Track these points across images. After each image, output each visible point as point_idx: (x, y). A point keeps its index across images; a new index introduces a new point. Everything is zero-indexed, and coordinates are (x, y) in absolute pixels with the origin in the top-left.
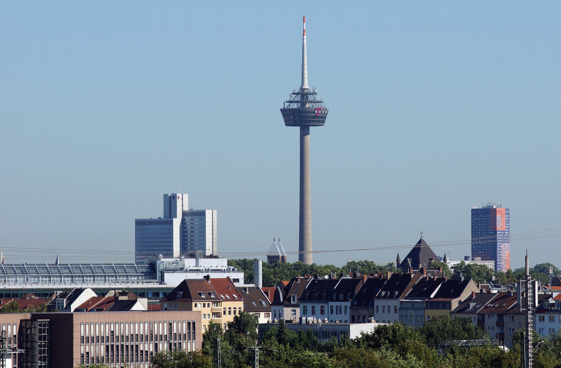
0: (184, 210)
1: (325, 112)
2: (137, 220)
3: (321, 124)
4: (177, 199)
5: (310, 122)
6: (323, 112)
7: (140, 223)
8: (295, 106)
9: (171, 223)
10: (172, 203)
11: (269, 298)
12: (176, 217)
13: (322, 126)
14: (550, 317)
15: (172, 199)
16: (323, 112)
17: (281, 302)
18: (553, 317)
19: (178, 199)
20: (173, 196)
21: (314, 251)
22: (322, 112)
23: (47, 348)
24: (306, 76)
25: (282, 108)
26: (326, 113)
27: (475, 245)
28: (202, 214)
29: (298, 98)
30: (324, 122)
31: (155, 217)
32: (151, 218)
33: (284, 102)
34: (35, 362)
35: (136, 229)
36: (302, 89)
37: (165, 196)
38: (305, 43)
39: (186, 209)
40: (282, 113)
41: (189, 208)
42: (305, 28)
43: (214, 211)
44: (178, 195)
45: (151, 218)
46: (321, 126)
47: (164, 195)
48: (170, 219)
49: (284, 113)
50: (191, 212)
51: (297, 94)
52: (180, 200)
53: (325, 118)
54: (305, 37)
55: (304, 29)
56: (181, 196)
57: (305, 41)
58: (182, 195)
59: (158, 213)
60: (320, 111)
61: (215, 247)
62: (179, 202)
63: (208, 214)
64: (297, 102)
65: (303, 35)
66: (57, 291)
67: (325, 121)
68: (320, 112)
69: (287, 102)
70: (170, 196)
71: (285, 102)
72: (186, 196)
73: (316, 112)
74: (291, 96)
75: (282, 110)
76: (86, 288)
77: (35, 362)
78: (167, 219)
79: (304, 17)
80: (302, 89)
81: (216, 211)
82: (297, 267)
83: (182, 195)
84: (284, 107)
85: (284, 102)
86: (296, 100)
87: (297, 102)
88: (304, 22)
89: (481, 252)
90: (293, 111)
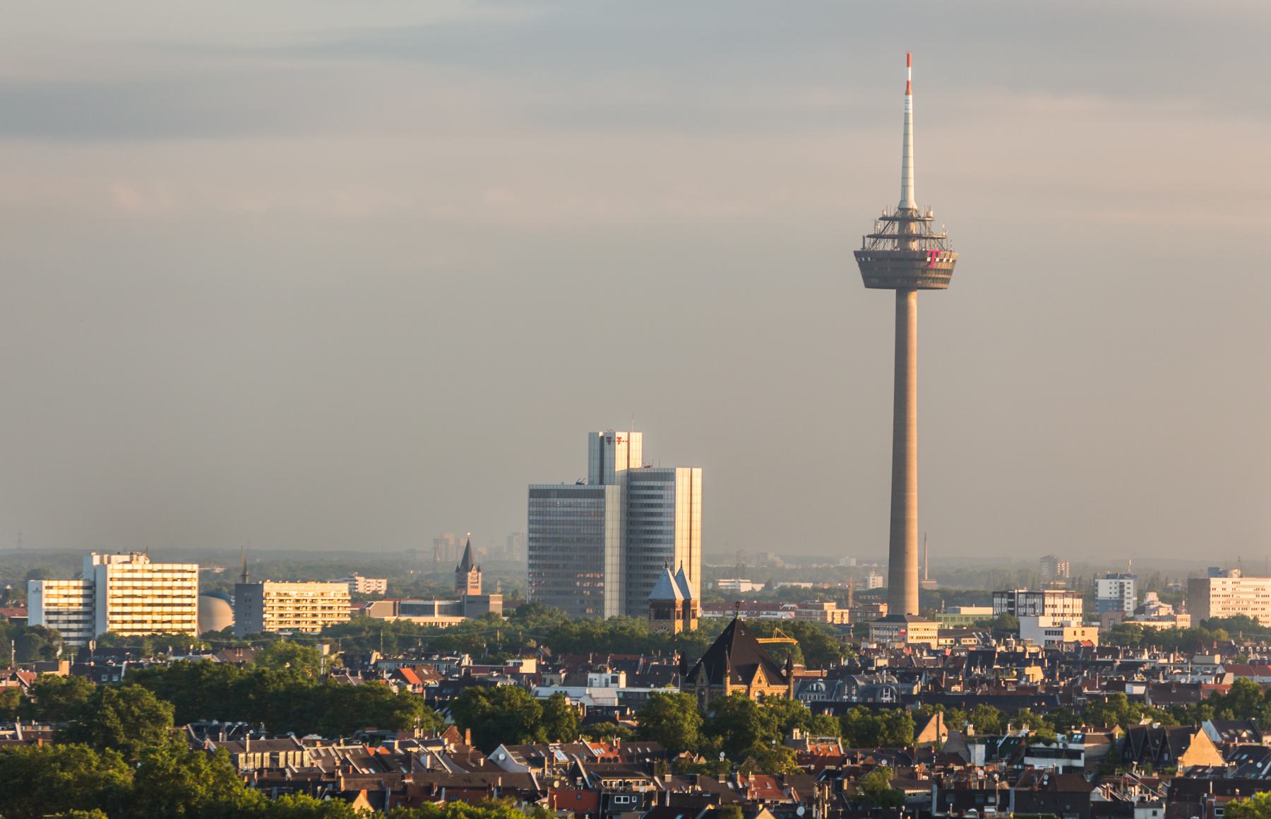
0: (631, 467)
2: (531, 488)
3: (944, 286)
4: (617, 443)
6: (945, 260)
7: (535, 493)
8: (887, 246)
10: (607, 454)
11: (351, 767)
15: (606, 443)
16: (945, 260)
18: (477, 587)
19: (609, 444)
20: (608, 438)
24: (911, 182)
25: (859, 248)
28: (669, 476)
29: (895, 229)
30: (947, 281)
31: (570, 482)
32: (563, 483)
34: (1012, 631)
37: (592, 436)
38: (911, 111)
40: (857, 260)
41: (643, 463)
42: (910, 79)
43: (694, 470)
44: (618, 434)
45: (563, 483)
47: (590, 434)
48: (600, 487)
49: (861, 260)
50: (646, 471)
51: (892, 220)
52: (624, 445)
55: (908, 82)
57: (911, 106)
59: (576, 472)
60: (937, 257)
61: (696, 548)
62: (620, 449)
63: (682, 475)
64: (892, 237)
65: (907, 93)
68: (937, 260)
69: (869, 236)
70: (602, 437)
72: (637, 438)
74: (876, 224)
75: (858, 254)
76: (681, 567)
77: (1012, 631)
78: (592, 487)
79: (908, 55)
80: (904, 209)
84: (864, 248)
87: (892, 237)
88: (908, 66)
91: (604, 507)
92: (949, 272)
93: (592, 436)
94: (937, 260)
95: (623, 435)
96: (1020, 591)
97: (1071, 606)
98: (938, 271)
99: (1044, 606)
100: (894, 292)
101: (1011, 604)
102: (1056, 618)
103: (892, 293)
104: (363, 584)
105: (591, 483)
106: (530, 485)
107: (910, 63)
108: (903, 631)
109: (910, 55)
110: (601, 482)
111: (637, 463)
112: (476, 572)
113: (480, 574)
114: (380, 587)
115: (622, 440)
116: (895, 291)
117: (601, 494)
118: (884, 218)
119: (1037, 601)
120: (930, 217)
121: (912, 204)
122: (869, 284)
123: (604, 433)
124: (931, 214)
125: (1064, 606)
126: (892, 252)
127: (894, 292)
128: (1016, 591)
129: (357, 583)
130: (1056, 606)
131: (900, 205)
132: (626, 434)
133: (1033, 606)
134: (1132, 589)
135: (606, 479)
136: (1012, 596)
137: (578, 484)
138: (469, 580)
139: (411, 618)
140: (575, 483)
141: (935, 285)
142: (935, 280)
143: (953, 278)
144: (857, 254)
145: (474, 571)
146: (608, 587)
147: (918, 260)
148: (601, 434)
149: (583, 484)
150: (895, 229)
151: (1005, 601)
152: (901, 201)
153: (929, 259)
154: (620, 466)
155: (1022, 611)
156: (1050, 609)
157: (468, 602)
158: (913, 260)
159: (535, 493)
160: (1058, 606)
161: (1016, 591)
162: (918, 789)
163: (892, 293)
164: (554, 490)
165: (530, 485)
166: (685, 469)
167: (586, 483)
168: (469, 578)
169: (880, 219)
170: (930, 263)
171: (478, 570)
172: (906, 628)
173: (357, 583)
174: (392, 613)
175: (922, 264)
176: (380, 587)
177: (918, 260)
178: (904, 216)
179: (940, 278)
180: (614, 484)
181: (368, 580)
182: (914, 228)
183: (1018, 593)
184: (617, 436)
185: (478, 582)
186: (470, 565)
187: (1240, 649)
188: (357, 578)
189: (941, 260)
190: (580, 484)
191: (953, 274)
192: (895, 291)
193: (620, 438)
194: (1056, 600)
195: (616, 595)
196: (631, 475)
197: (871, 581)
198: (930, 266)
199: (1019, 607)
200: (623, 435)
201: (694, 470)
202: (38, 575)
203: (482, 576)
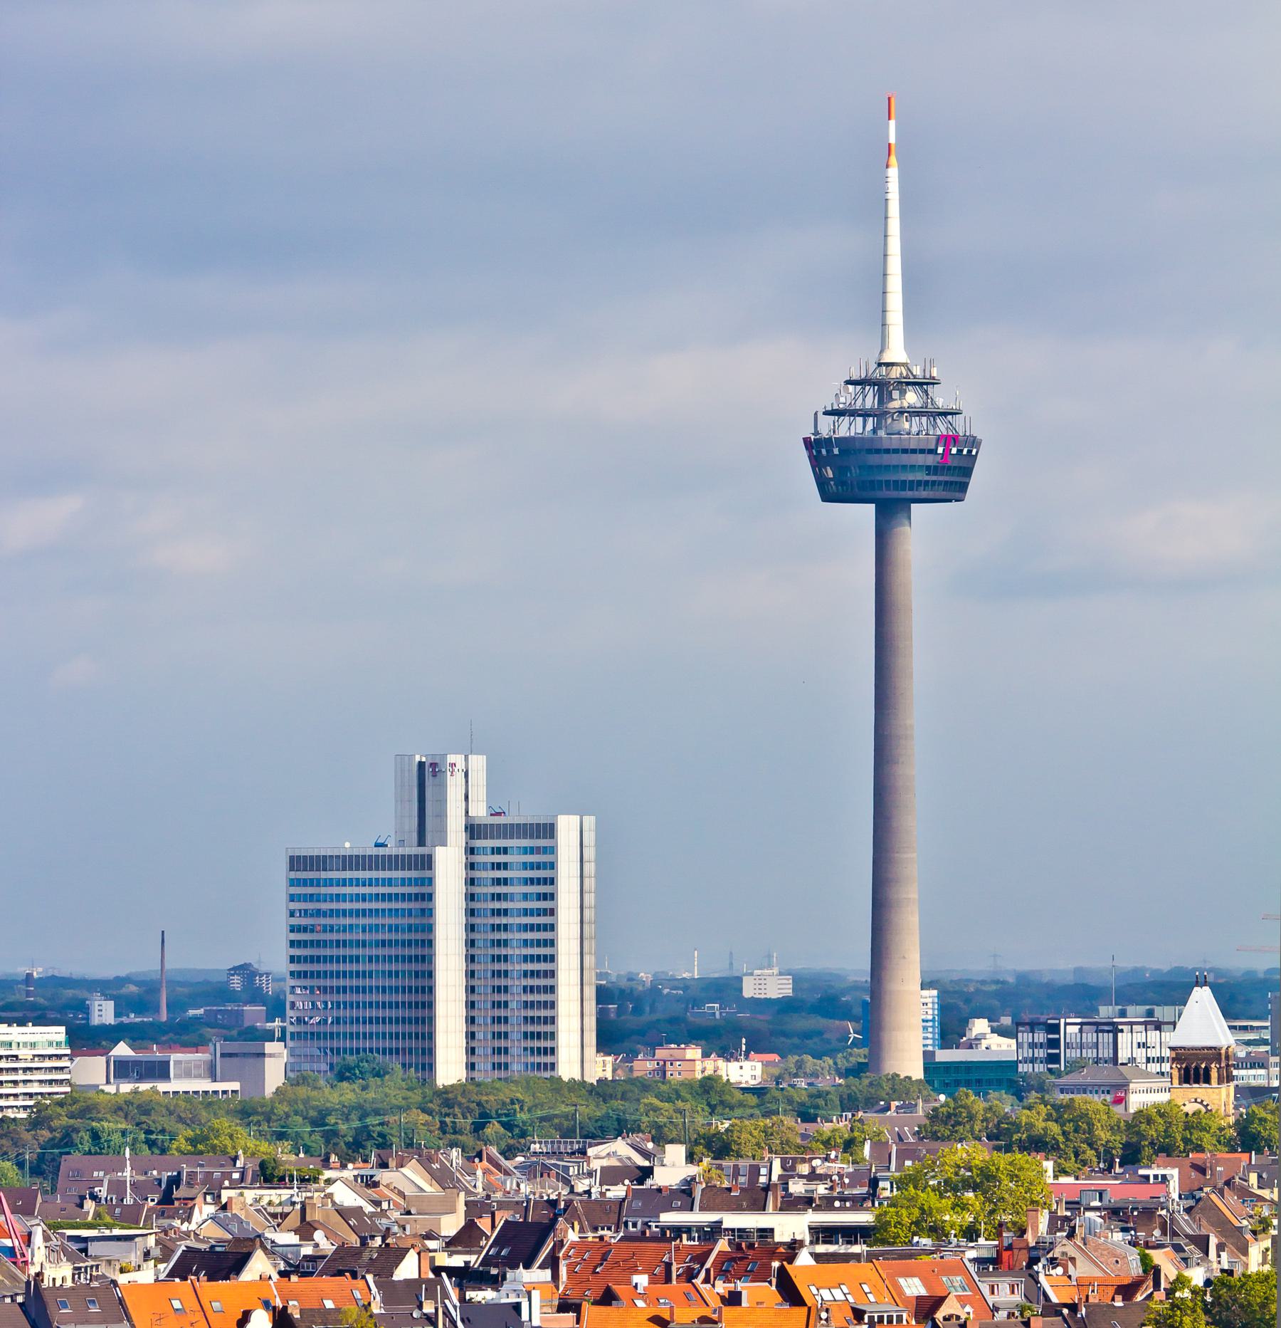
0: (470, 814)
1: (970, 451)
3: (958, 495)
4: (449, 773)
7: (297, 863)
8: (848, 428)
9: (427, 862)
12: (444, 844)
13: (954, 504)
21: (251, 1061)
22: (962, 451)
23: (697, 1243)
26: (974, 453)
27: (928, 1063)
30: (963, 487)
33: (816, 414)
39: (479, 811)
42: (892, 140)
43: (585, 818)
44: (451, 758)
46: (950, 501)
48: (421, 850)
52: (460, 776)
53: (968, 472)
55: (890, 145)
56: (461, 764)
63: (567, 828)
67: (967, 484)
68: (954, 451)
69: (826, 413)
71: (820, 415)
72: (478, 763)
73: (940, 450)
81: (593, 818)
82: (613, 1081)
84: (816, 433)
85: (816, 414)
88: (889, 119)
89: (95, 1174)
97: (1135, 1045)
105: (401, 843)
107: (893, 115)
110: (421, 842)
116: (873, 506)
122: (823, 500)
125: (1096, 1045)
127: (871, 508)
134: (96, 1011)
139: (155, 1084)
148: (418, 758)
150: (870, 400)
151: (1040, 1037)
157: (223, 1055)
161: (1062, 1021)
162: (545, 1258)
174: (1069, 1200)
190: (498, 814)
192: (873, 506)
193: (453, 765)
194: (1036, 1035)
197: (97, 1008)
200: (458, 759)
202: (1197, 984)
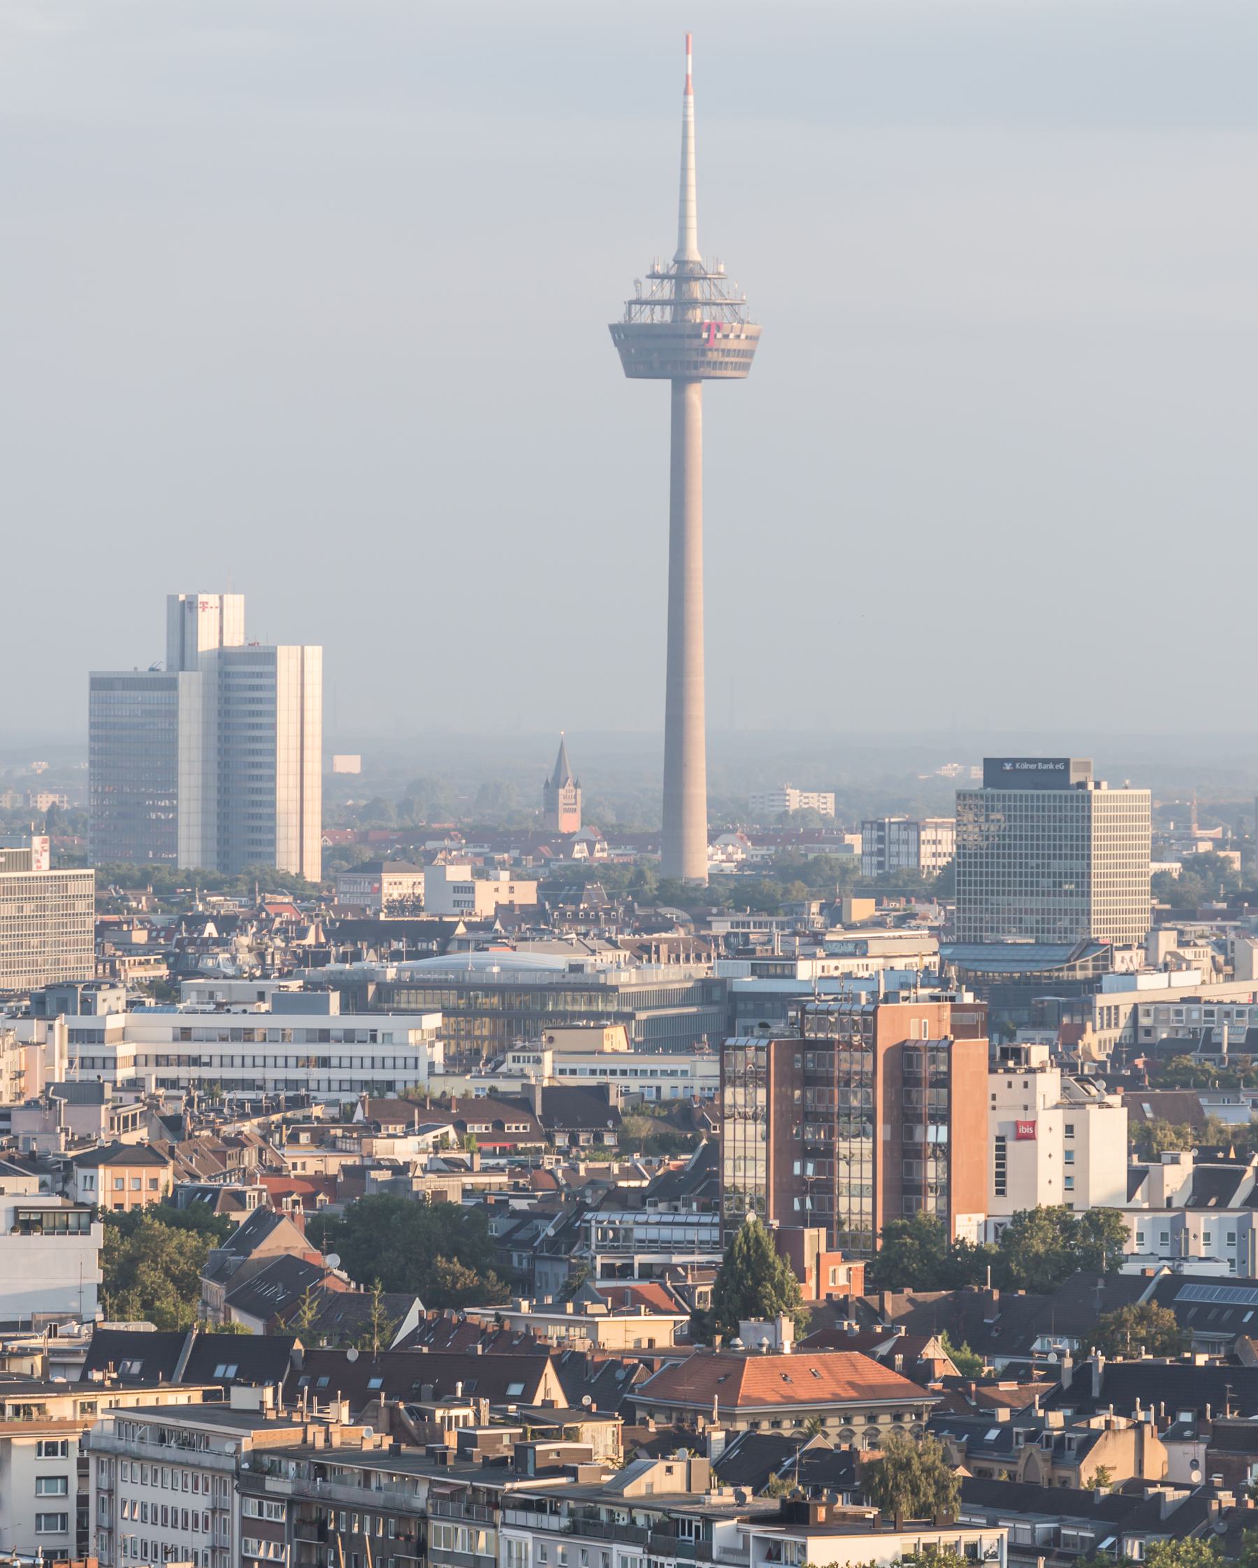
0: (225, 644)
4: (200, 610)
5: (696, 368)
6: (732, 336)
7: (100, 684)
8: (662, 316)
10: (188, 625)
14: (566, 811)
15: (187, 610)
17: (1121, 1272)
18: (575, 810)
19: (203, 610)
24: (693, 222)
25: (618, 317)
28: (269, 657)
29: (666, 291)
30: (746, 367)
35: (90, 703)
36: (681, 262)
38: (691, 119)
41: (246, 638)
42: (690, 72)
43: (308, 649)
44: (202, 598)
51: (663, 277)
54: (691, 98)
55: (687, 76)
57: (691, 111)
58: (221, 598)
60: (719, 331)
63: (287, 659)
65: (686, 93)
66: (256, 1516)
68: (719, 335)
80: (681, 262)
83: (221, 598)
86: (658, 296)
90: (649, 331)
91: (177, 704)
92: (749, 354)
93: (172, 599)
94: (719, 335)
95: (213, 599)
96: (892, 820)
98: (726, 352)
99: (919, 842)
100: (668, 382)
101: (881, 840)
102: (939, 859)
103: (667, 384)
104: (798, 799)
106: (91, 673)
108: (377, 885)
109: (690, 36)
111: (235, 638)
112: (572, 788)
113: (579, 791)
114: (825, 803)
115: (209, 605)
117: (171, 685)
118: (653, 276)
119: (913, 835)
120: (719, 274)
121: (694, 254)
123: (187, 596)
124: (722, 269)
126: (662, 325)
127: (668, 382)
128: (887, 820)
129: (787, 798)
130: (940, 842)
131: (675, 256)
132: (217, 597)
133: (906, 842)
135: (188, 663)
136: (881, 827)
137: (152, 670)
138: (561, 800)
140: (147, 670)
141: (718, 373)
142: (722, 365)
143: (756, 362)
144: (614, 329)
145: (569, 786)
146: (183, 820)
147: (689, 336)
148: (182, 597)
149: (158, 670)
150: (666, 291)
152: (678, 251)
153: (705, 335)
154: (207, 641)
155: (894, 848)
156: (928, 847)
158: (682, 336)
159: (100, 684)
160: (944, 842)
163: (667, 384)
164: (119, 679)
165: (91, 673)
166: (291, 647)
167: (163, 668)
168: (561, 797)
169: (648, 277)
170: (707, 340)
171: (576, 786)
172: (380, 881)
173: (787, 798)
175: (696, 342)
176: (825, 803)
177: (689, 336)
178: (683, 274)
179: (732, 363)
180: (196, 670)
181: (805, 794)
182: (698, 290)
183: (890, 823)
184: (200, 600)
185: (576, 804)
186: (562, 780)
187: (553, 915)
188: (789, 791)
189: (726, 337)
191: (755, 356)
195: (196, 831)
196: (224, 656)
198: (708, 346)
199: (890, 843)
201: (308, 649)
203: (583, 795)
